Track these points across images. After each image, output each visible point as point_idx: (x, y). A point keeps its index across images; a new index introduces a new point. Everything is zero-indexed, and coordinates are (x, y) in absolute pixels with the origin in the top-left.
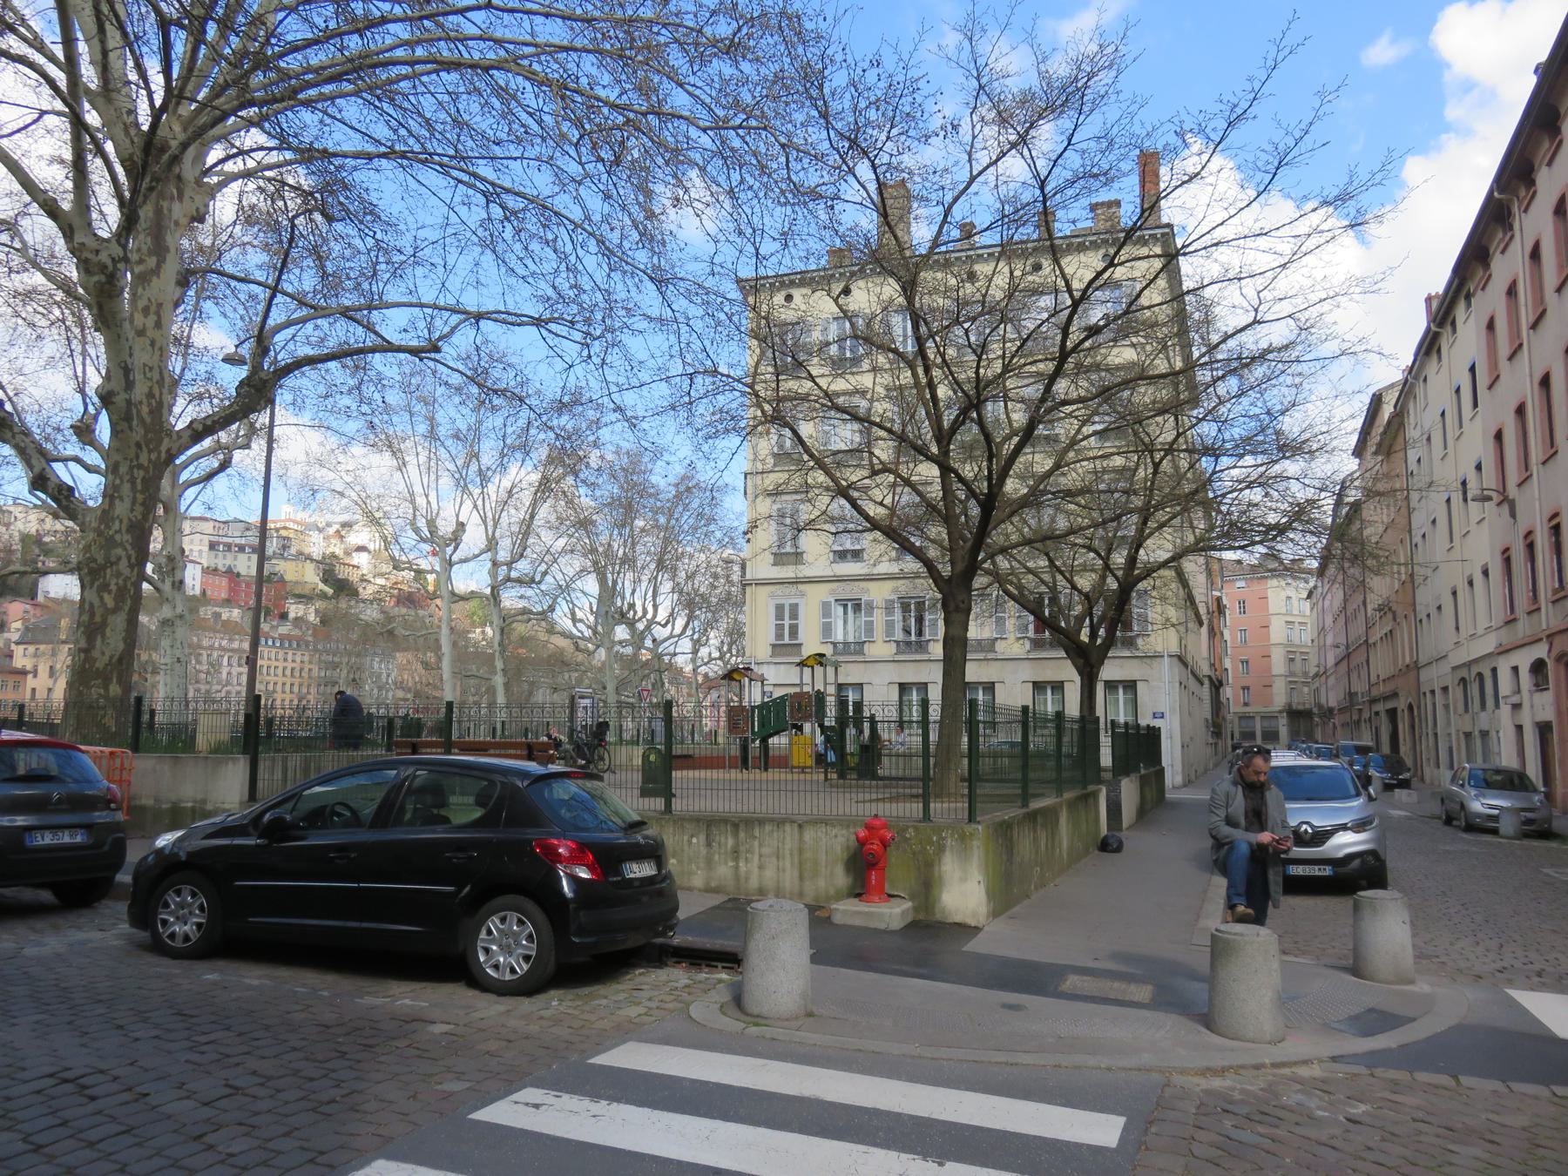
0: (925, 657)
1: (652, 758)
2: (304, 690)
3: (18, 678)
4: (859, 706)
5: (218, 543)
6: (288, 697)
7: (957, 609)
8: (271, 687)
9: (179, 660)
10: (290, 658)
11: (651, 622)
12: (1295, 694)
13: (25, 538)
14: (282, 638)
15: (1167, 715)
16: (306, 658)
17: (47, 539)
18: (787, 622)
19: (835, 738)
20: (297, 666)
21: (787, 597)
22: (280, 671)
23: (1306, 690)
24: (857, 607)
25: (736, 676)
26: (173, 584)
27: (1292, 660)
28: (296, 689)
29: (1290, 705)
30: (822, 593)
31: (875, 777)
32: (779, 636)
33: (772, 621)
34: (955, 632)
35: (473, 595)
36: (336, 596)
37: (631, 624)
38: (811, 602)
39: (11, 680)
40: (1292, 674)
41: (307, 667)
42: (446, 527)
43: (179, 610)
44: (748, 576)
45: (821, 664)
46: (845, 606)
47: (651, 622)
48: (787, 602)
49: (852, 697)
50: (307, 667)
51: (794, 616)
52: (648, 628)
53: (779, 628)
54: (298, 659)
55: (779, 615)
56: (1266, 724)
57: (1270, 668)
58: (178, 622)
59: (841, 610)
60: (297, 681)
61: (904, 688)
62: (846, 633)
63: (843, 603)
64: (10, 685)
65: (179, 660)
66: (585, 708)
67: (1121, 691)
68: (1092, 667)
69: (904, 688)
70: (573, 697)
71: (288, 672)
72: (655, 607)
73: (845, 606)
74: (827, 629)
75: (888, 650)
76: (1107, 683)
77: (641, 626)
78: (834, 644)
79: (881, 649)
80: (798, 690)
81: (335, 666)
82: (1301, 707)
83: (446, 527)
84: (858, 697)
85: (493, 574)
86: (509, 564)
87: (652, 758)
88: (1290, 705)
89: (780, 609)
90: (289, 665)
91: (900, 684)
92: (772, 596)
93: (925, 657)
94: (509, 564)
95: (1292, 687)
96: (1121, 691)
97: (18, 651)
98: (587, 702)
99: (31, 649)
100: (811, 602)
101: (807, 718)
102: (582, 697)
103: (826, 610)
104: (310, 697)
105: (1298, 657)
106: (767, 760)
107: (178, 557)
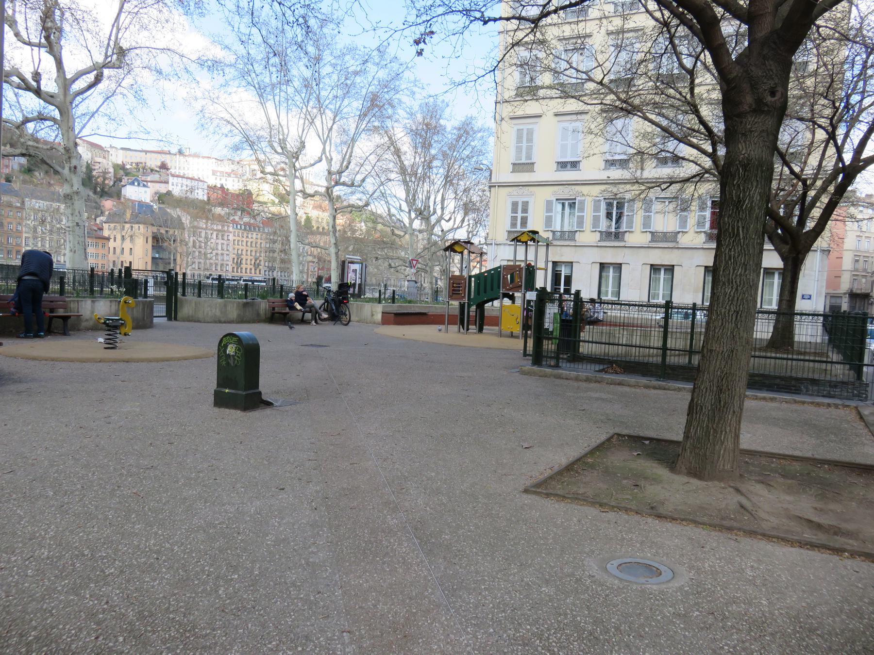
0: (622, 244)
1: (231, 350)
2: (258, 255)
3: (104, 241)
4: (568, 280)
5: (217, 172)
6: (249, 258)
7: (759, 108)
8: (240, 252)
9: (78, 224)
10: (250, 236)
11: (441, 218)
12: (856, 282)
13: (116, 167)
14: (245, 224)
15: (814, 297)
16: (259, 236)
17: (128, 167)
18: (520, 215)
19: (533, 319)
20: (254, 240)
21: (520, 195)
22: (244, 244)
23: (864, 280)
24: (572, 205)
25: (457, 248)
26: (70, 169)
27: (857, 261)
28: (253, 254)
29: (852, 290)
30: (548, 193)
31: (577, 358)
32: (514, 225)
33: (509, 214)
34: (750, 150)
35: (317, 193)
36: (281, 203)
37: (426, 219)
38: (538, 200)
39: (100, 242)
40: (856, 270)
41: (259, 241)
42: (292, 144)
43: (75, 188)
44: (493, 180)
45: (533, 240)
46: (563, 205)
47: (441, 218)
48: (520, 200)
49: (564, 271)
50: (259, 241)
51: (525, 210)
52: (438, 221)
53: (514, 219)
54: (254, 236)
55: (514, 210)
56: (833, 301)
57: (841, 266)
58: (76, 198)
59: (560, 207)
60: (254, 249)
61: (603, 266)
62: (562, 226)
63: (562, 201)
64: (100, 245)
65: (78, 224)
66: (355, 271)
67: (662, 272)
68: (798, 253)
69: (603, 266)
70: (344, 262)
71: (249, 244)
72: (443, 208)
73: (563, 205)
74: (549, 221)
75: (595, 238)
76: (765, 269)
77: (433, 219)
78: (554, 232)
79: (588, 237)
80: (511, 263)
81: (274, 242)
82: (859, 292)
83: (292, 144)
84: (568, 272)
85: (328, 179)
86: (340, 173)
87: (231, 350)
88: (852, 290)
89: (515, 205)
90: (250, 240)
91: (601, 264)
92: (510, 195)
93: (622, 244)
94: (340, 173)
95: (855, 278)
96: (662, 272)
97: (106, 226)
98: (357, 267)
99: (112, 225)
100: (538, 200)
101: (518, 288)
102: (352, 263)
103: (549, 204)
104: (261, 258)
105: (862, 259)
106: (482, 321)
107: (73, 149)
